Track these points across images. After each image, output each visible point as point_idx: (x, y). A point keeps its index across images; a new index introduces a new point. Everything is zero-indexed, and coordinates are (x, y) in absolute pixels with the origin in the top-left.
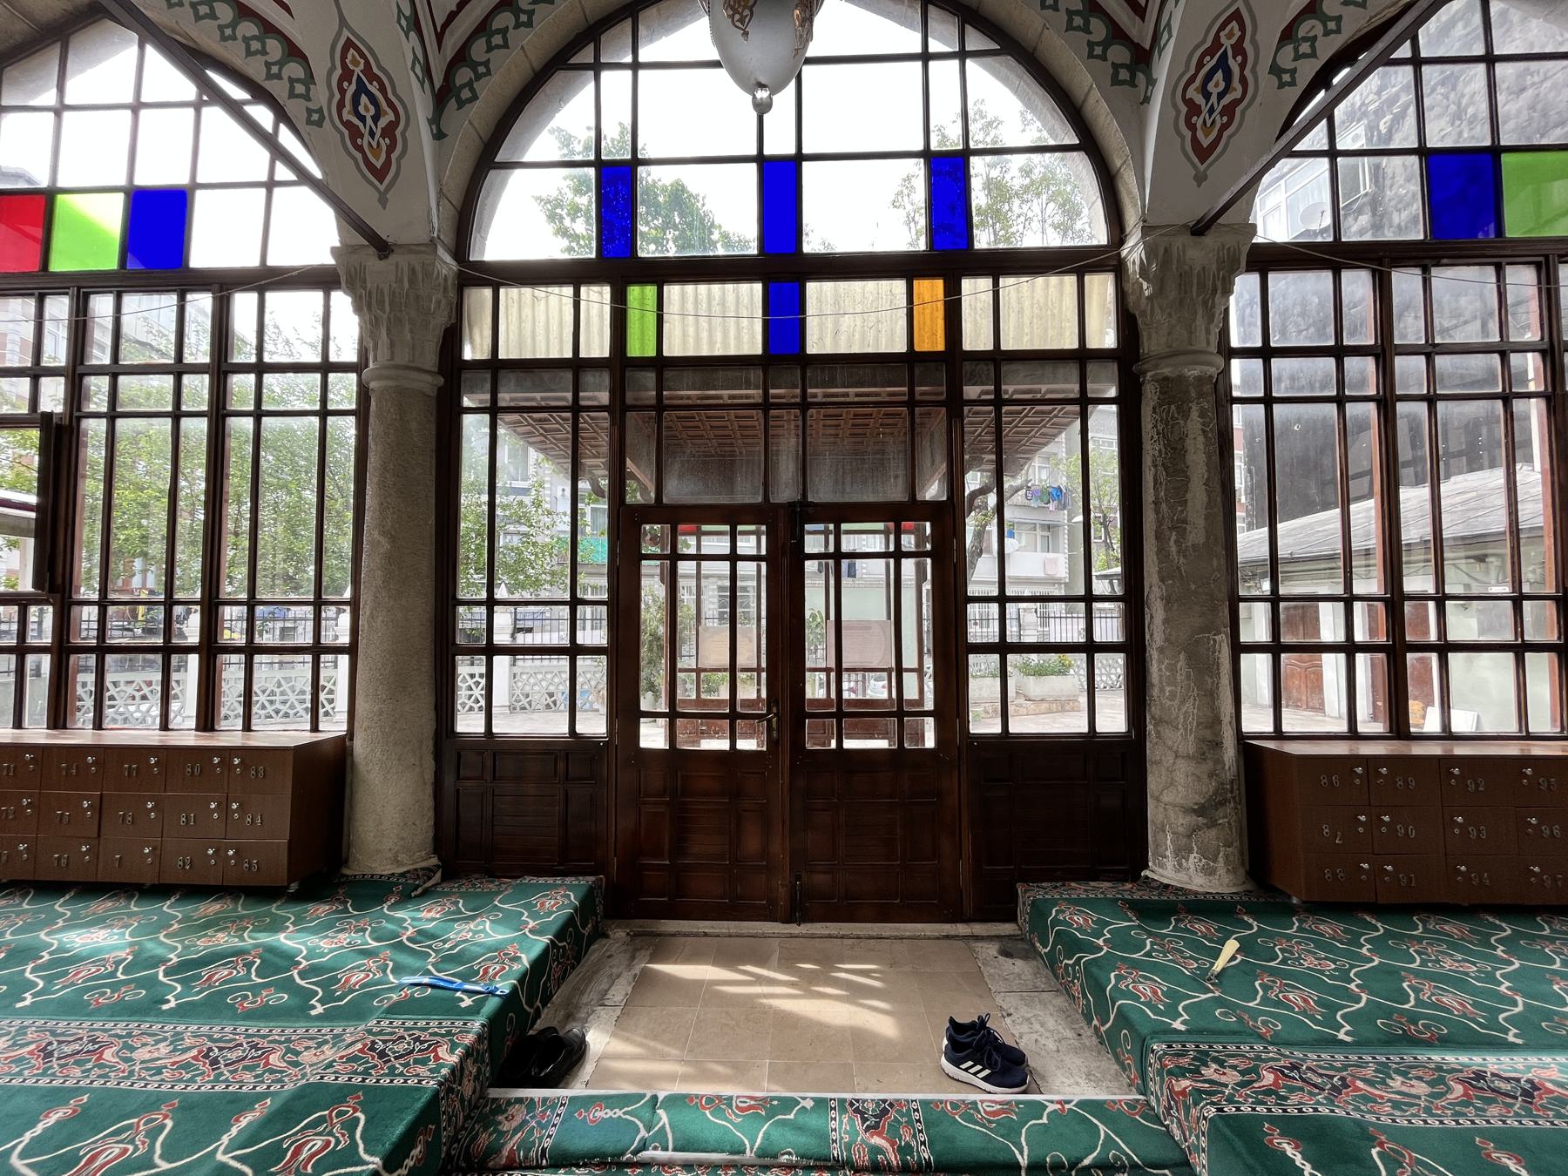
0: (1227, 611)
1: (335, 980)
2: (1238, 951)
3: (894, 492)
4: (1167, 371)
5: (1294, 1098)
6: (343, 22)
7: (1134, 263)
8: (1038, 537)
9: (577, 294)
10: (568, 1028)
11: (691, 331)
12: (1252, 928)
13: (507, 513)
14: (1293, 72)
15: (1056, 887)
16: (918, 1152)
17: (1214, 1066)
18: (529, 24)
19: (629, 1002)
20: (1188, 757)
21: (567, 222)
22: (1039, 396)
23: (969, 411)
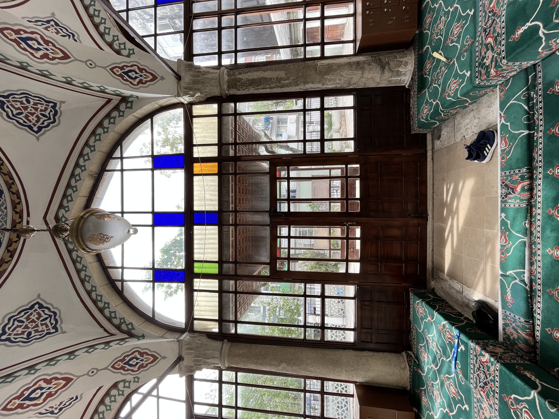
0: (309, 62)
1: (454, 398)
2: (438, 52)
3: (266, 180)
5: (498, 30)
6: (106, 368)
7: (189, 99)
8: (282, 125)
9: (196, 291)
10: (473, 307)
11: (210, 251)
12: (428, 47)
13: (272, 315)
14: (130, 50)
15: (413, 119)
16: (523, 173)
17: (485, 60)
18: (108, 304)
19: (461, 282)
20: (363, 73)
21: (173, 290)
22: (233, 130)
23: (239, 153)
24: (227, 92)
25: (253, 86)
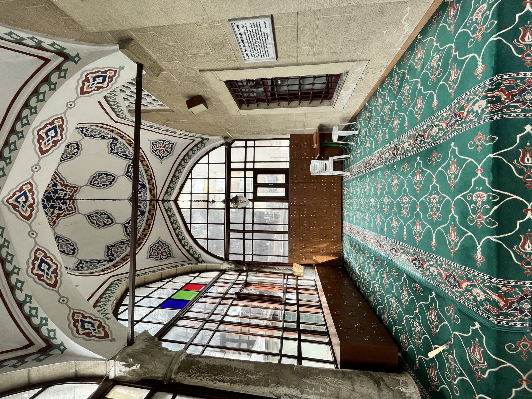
4: (176, 367)
17: (478, 299)
24: (173, 376)
25: (209, 374)
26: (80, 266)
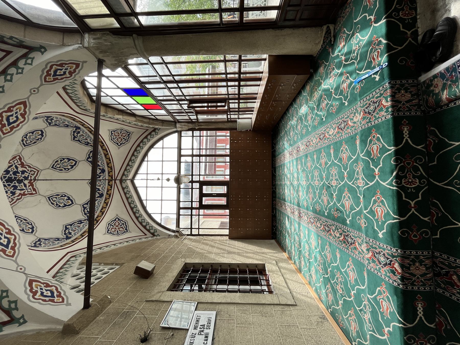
26: (37, 244)
